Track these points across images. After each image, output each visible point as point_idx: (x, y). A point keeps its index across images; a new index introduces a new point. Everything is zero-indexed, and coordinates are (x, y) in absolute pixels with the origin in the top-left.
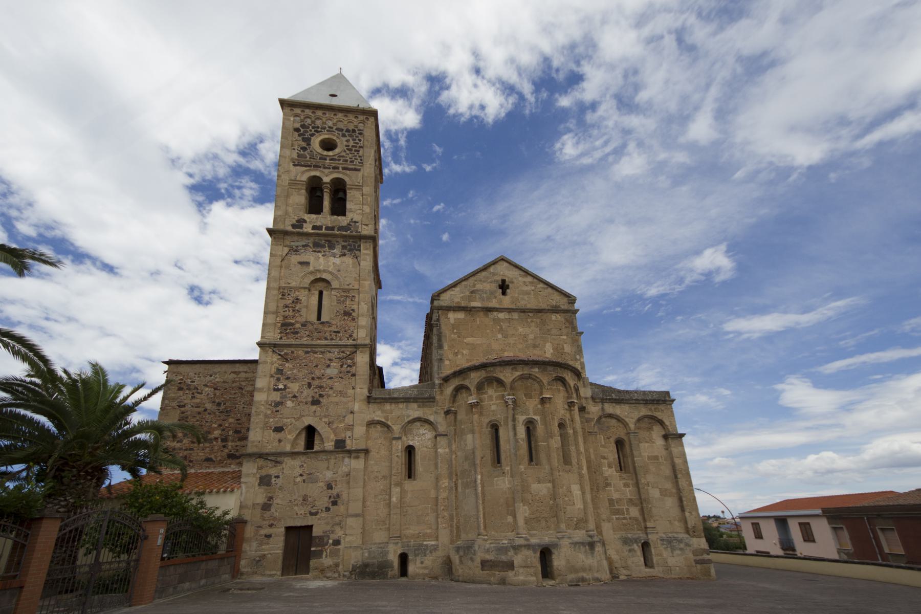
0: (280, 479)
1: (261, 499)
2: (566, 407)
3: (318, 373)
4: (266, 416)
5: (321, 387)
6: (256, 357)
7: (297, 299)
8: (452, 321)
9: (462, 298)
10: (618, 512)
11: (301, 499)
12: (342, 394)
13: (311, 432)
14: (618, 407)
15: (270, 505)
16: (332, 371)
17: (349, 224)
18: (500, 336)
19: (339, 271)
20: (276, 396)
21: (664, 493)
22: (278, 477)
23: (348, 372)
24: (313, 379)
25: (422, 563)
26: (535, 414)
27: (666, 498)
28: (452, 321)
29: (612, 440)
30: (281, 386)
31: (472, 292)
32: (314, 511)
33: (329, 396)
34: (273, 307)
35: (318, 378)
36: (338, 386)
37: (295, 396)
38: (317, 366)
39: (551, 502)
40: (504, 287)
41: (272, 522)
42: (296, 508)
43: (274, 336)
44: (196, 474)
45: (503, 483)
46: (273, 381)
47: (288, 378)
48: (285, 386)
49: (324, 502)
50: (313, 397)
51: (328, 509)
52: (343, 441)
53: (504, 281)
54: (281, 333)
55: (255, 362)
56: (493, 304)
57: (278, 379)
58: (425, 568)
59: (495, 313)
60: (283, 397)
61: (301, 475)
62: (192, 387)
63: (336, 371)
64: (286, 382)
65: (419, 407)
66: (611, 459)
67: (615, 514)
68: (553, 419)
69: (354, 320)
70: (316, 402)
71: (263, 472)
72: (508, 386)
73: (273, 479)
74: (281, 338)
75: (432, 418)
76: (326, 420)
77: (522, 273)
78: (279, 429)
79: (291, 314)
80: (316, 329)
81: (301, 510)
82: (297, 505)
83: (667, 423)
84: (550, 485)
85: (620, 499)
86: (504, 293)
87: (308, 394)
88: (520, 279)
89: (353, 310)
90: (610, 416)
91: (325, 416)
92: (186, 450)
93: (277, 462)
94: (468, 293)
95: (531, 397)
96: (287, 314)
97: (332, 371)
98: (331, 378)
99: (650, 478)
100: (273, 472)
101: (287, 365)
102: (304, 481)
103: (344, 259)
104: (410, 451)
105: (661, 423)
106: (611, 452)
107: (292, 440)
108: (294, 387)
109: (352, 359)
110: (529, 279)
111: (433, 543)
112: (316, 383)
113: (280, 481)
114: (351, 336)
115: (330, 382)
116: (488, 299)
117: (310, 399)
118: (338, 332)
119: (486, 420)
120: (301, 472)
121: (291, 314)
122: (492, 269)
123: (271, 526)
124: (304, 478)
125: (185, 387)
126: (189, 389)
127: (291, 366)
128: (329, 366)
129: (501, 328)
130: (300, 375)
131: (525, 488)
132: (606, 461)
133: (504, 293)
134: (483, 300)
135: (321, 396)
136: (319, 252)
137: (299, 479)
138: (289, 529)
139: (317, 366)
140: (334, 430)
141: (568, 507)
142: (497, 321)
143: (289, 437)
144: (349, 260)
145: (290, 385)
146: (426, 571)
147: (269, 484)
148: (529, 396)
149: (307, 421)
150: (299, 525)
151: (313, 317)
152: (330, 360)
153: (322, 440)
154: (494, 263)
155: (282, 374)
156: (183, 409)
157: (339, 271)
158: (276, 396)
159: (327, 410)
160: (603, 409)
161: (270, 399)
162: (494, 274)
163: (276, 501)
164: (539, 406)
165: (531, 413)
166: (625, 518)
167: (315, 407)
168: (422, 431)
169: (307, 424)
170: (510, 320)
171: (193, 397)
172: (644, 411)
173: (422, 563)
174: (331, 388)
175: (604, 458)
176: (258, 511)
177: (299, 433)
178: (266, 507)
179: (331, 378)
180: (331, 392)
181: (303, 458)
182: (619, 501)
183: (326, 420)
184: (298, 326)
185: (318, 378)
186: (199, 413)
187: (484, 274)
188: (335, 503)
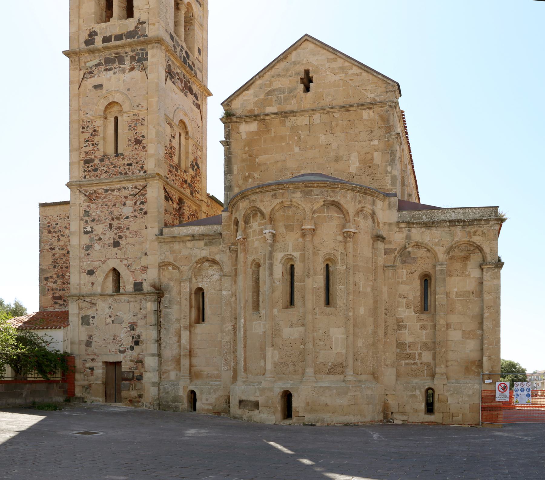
0: (96, 319)
1: (84, 338)
2: (340, 238)
3: (116, 213)
4: (81, 260)
5: (119, 228)
6: (67, 198)
7: (95, 131)
8: (244, 136)
9: (255, 103)
10: (410, 357)
11: (112, 338)
12: (136, 233)
13: (116, 273)
14: (428, 232)
15: (91, 342)
16: (128, 210)
17: (136, 27)
18: (297, 150)
19: (129, 90)
20: (86, 240)
21: (466, 335)
22: (93, 317)
23: (141, 210)
24: (113, 219)
25: (207, 400)
26: (294, 250)
27: (468, 341)
28: (244, 136)
29: (416, 275)
30: (89, 229)
31: (269, 94)
32: (122, 349)
33: (126, 237)
34: (76, 145)
35: (118, 218)
36: (134, 226)
37: (100, 239)
38: (115, 205)
39: (302, 347)
40: (307, 81)
41: (93, 357)
42: (109, 346)
43: (79, 173)
44: (403, 272)
45: (259, 327)
46: (83, 223)
47: (93, 220)
48: (92, 228)
49: (128, 342)
50: (114, 239)
51: (132, 348)
52: (141, 284)
53: (307, 72)
54: (85, 171)
55: (67, 203)
56: (292, 106)
57: (86, 222)
58: (210, 404)
59: (293, 118)
60: (91, 240)
61: (110, 316)
62: (57, 230)
63: (131, 209)
64: (93, 225)
65: (206, 245)
66: (411, 298)
67: (405, 359)
68: (315, 254)
69: (144, 148)
70: (116, 244)
71: (83, 313)
72: (267, 217)
73: (91, 319)
74: (85, 177)
75: (217, 258)
76: (125, 262)
77: (332, 56)
78: (91, 273)
79: (90, 148)
80: (112, 164)
81: (113, 348)
82: (109, 343)
83: (487, 250)
84: (301, 329)
85: (414, 343)
86: (307, 89)
87: (110, 236)
88: (327, 65)
89: (143, 136)
90: (418, 245)
91: (126, 259)
92: (60, 290)
93: (92, 303)
94: (262, 96)
95: (292, 230)
96: (87, 149)
97: (128, 210)
98: (127, 218)
99: (454, 319)
100: (90, 313)
101: (92, 206)
102: (113, 322)
103: (134, 73)
104: (200, 292)
105: (480, 249)
106: (413, 290)
107: (102, 282)
108: (99, 229)
109: (144, 195)
110: (340, 62)
111: (218, 383)
112: (115, 223)
113: (95, 321)
114: (142, 167)
115: (126, 222)
116: (286, 99)
117: (112, 241)
118: (130, 165)
119: (250, 259)
120: (110, 314)
121: (90, 148)
122: (293, 57)
123: (93, 360)
124: (113, 319)
125: (52, 230)
126: (55, 232)
127: (95, 207)
128: (124, 205)
129: (299, 139)
130: (103, 216)
131: (276, 332)
132: (404, 300)
133: (307, 89)
134: (280, 103)
135: (120, 237)
136: (110, 70)
137: (109, 320)
138: (106, 363)
139: (115, 205)
140: (132, 272)
141: (322, 352)
142: (294, 129)
143: (99, 279)
144: (137, 74)
145: (96, 227)
146: (211, 408)
147: (88, 324)
148: (289, 228)
149: (112, 264)
150: (111, 361)
151: (110, 150)
152: (126, 197)
153: (124, 282)
154: (295, 47)
155: (88, 216)
156: (53, 251)
157: (129, 90)
158: (86, 240)
159: (126, 252)
160: (408, 238)
161: (82, 242)
162: (295, 63)
163: (95, 339)
164: (301, 240)
165: (291, 248)
166: (415, 364)
167: (116, 249)
168: (210, 272)
169: (111, 267)
170: (310, 127)
171: (59, 240)
172: (459, 234)
173: (207, 400)
174: (128, 229)
175: (403, 296)
176: (83, 347)
177: (107, 276)
178: (88, 344)
179: (127, 218)
180: (128, 233)
181: (110, 300)
182: (412, 345)
183: (125, 262)
184: (97, 161)
185: (118, 218)
186: (64, 255)
187: (282, 65)
188: (137, 343)
